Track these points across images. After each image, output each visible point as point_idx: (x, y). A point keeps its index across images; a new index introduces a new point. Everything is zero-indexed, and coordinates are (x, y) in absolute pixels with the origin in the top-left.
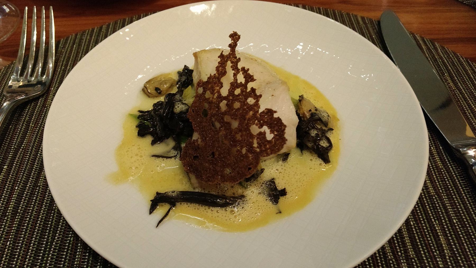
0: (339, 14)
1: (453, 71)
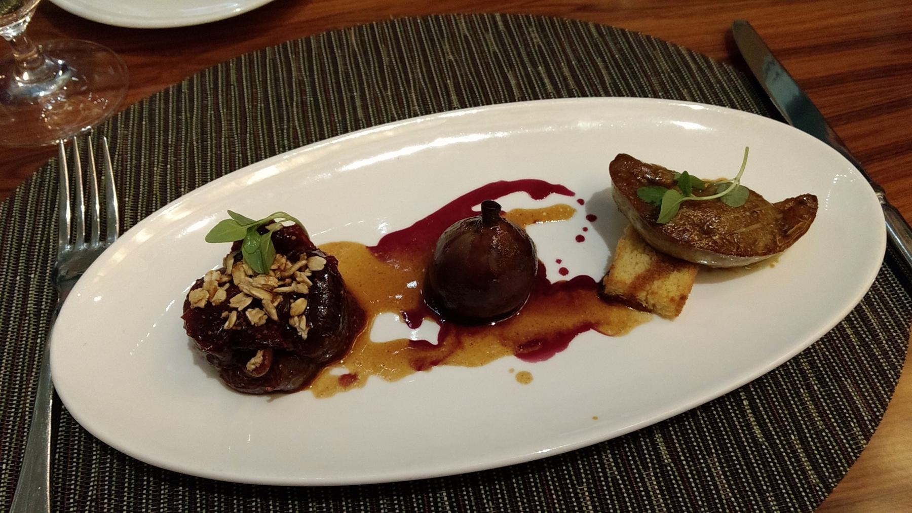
0: (560, 23)
1: (737, 100)
